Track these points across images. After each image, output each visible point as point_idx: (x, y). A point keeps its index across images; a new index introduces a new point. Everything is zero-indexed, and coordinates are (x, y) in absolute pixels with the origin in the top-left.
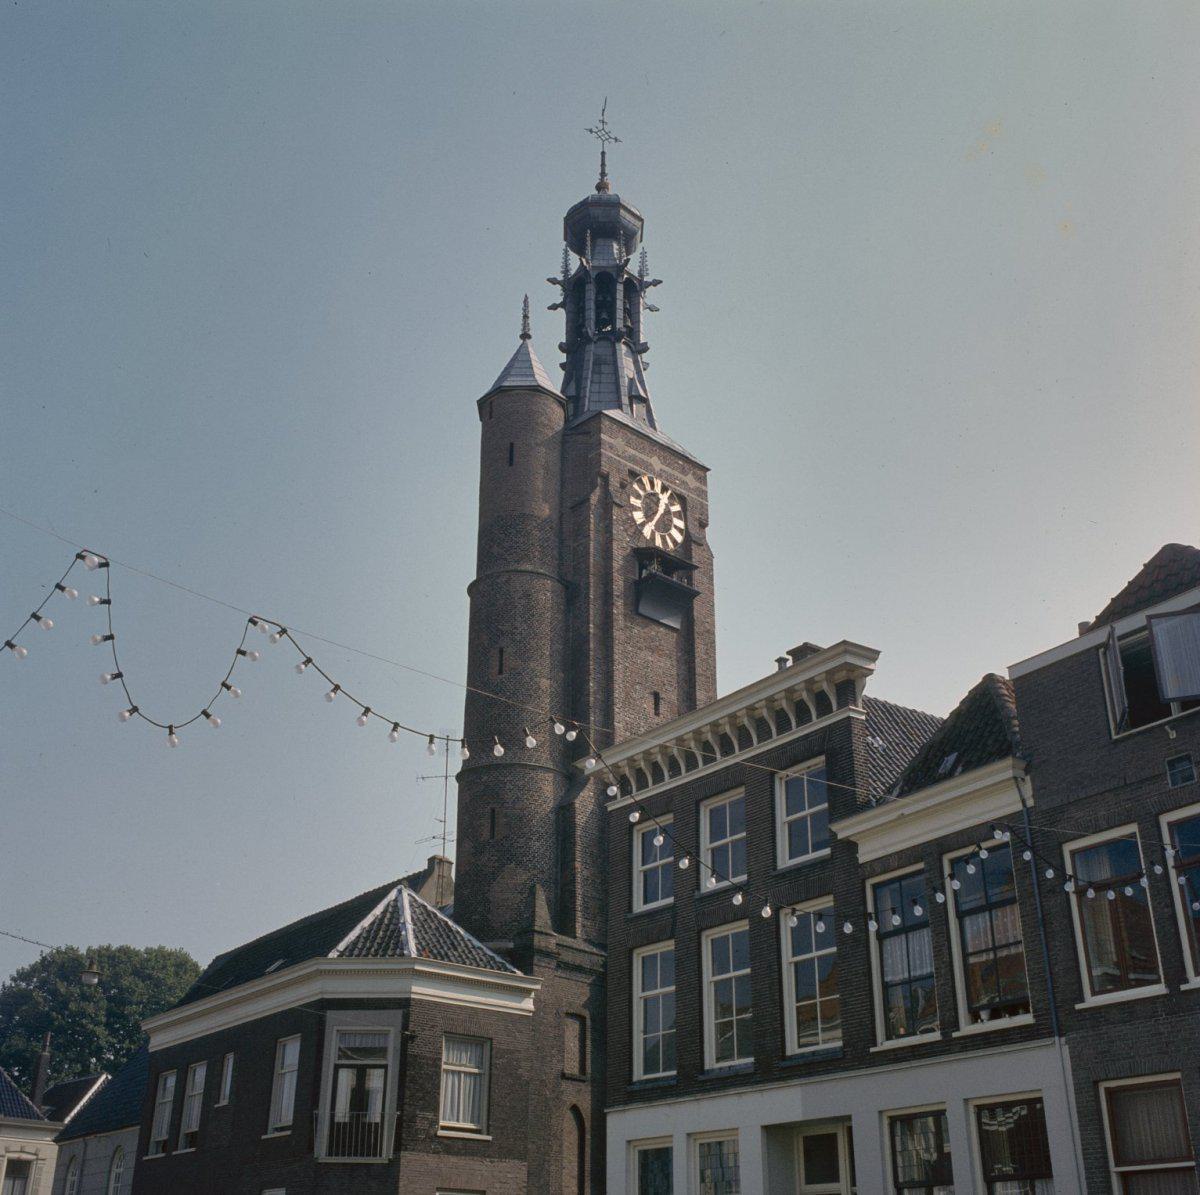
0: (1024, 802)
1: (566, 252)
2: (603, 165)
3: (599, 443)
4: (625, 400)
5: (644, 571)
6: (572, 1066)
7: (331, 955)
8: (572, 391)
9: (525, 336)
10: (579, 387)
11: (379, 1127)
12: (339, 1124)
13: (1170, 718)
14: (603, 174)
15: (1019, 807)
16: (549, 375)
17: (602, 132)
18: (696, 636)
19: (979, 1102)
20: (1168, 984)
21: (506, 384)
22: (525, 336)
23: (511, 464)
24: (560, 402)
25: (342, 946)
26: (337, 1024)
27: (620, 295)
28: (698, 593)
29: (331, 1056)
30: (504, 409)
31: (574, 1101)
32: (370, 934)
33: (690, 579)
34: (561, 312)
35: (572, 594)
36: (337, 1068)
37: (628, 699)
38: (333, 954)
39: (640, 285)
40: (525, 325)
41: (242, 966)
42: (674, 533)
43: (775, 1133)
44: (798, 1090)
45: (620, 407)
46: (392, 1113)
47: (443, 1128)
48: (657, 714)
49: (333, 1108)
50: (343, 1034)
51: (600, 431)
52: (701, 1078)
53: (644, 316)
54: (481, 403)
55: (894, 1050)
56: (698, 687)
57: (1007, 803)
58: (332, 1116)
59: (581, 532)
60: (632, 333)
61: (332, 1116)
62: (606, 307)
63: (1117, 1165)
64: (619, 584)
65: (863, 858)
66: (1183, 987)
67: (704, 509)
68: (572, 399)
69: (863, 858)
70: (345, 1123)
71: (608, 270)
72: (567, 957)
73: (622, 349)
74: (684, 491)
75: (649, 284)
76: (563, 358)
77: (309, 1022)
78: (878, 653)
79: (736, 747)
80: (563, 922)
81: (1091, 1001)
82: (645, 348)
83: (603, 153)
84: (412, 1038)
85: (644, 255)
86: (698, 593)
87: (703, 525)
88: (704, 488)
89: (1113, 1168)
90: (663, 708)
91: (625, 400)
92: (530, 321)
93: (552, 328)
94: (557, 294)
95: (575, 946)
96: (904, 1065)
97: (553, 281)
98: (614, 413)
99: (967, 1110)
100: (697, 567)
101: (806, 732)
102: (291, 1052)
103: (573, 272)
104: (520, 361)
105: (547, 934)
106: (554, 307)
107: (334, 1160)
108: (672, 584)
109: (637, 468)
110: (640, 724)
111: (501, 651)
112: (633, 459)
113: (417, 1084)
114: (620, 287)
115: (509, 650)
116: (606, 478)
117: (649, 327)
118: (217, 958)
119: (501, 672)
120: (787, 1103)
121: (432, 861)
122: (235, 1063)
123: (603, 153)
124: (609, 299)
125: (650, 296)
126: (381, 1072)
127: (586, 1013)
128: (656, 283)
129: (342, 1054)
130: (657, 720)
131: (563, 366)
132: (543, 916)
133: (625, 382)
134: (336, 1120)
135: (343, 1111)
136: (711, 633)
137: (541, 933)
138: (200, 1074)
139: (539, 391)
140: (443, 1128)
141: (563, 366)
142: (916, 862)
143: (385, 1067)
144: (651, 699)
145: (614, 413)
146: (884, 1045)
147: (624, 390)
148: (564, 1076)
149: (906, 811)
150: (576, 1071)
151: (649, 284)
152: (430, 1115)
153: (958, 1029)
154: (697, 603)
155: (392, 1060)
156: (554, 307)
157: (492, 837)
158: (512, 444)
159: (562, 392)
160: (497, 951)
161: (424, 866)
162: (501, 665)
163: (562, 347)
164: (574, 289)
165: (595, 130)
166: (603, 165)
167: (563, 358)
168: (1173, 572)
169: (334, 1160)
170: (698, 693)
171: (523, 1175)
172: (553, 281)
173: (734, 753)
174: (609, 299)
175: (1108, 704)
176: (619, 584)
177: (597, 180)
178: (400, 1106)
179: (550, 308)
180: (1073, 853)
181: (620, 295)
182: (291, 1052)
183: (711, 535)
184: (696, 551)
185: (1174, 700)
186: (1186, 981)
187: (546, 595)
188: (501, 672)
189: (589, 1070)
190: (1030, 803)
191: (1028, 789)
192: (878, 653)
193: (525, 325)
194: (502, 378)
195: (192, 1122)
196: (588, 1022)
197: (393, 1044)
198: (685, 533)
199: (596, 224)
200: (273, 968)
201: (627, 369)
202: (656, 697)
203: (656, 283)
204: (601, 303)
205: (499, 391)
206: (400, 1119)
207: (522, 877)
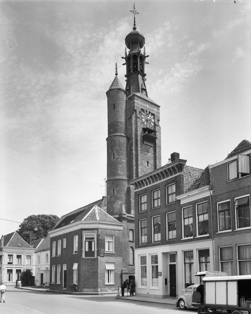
0: (211, 194)
1: (126, 49)
2: (135, 22)
3: (134, 102)
4: (140, 90)
5: (145, 133)
6: (131, 239)
7: (82, 220)
8: (128, 88)
9: (116, 74)
10: (130, 87)
11: (94, 252)
12: (86, 251)
13: (130, 275)
14: (135, 25)
15: (210, 195)
16: (123, 85)
17: (134, 12)
18: (157, 148)
19: (199, 249)
20: (232, 230)
21: (112, 88)
22: (116, 74)
23: (114, 109)
24: (125, 92)
25: (84, 218)
26: (85, 235)
27: (139, 61)
28: (157, 138)
29: (84, 240)
30: (112, 94)
31: (131, 246)
32: (90, 216)
33: (155, 134)
34: (125, 66)
35: (129, 139)
36: (85, 241)
37: (141, 163)
38: (83, 220)
39: (144, 57)
40: (116, 72)
41: (68, 219)
42: (152, 123)
43: (164, 254)
44: (169, 246)
45: (139, 92)
46: (96, 249)
47: (106, 252)
48: (148, 166)
49: (85, 249)
50: (86, 235)
51: (134, 99)
52: (151, 244)
53: (146, 66)
54: (107, 93)
55: (185, 240)
56: (157, 159)
57: (208, 194)
58: (85, 250)
59: (131, 124)
60: (142, 71)
61: (85, 250)
62: (135, 64)
63: (221, 261)
64: (139, 139)
65: (181, 203)
66: (235, 230)
67: (159, 117)
68: (128, 91)
69: (181, 203)
70: (87, 251)
71: (136, 54)
72: (129, 218)
73: (140, 77)
74: (154, 113)
75: (146, 57)
76: (126, 79)
77: (79, 232)
78: (186, 161)
79: (152, 183)
80: (128, 211)
81: (219, 232)
82: (145, 75)
83: (135, 18)
84: (99, 235)
85: (144, 48)
86: (157, 138)
87: (158, 121)
88: (159, 111)
89: (220, 261)
90: (149, 165)
91: (140, 90)
92: (117, 70)
93: (123, 70)
94: (124, 61)
95: (131, 216)
96: (187, 243)
97: (123, 58)
98: (138, 94)
99: (197, 251)
100: (157, 132)
101: (172, 177)
102: (76, 238)
103: (127, 55)
104: (116, 81)
105: (125, 214)
106: (124, 64)
107: (86, 258)
108: (150, 136)
109: (143, 108)
110: (144, 169)
111: (114, 154)
112: (142, 106)
113: (101, 244)
114: (139, 59)
115: (116, 154)
116: (136, 111)
117: (147, 69)
118: (125, 39)
119: (114, 159)
120: (167, 249)
121: (103, 197)
122: (67, 241)
123: (135, 18)
124: (136, 62)
125: (147, 60)
126: (94, 242)
127: (134, 229)
128: (148, 56)
129: (86, 239)
130: (148, 167)
131: (126, 80)
132: (124, 211)
133: (140, 85)
134: (86, 251)
135: (87, 250)
136: (160, 147)
137: (124, 214)
138: (60, 241)
139: (120, 90)
140: (106, 252)
141: (126, 80)
142: (191, 205)
143: (94, 241)
144: (147, 163)
145: (138, 94)
146: (183, 239)
147: (140, 87)
148: (130, 241)
149: (189, 195)
150: (132, 240)
151: (146, 57)
152: (103, 249)
153: (196, 236)
154: (157, 140)
155: (95, 240)
156: (124, 64)
157: (114, 194)
158: (114, 104)
159: (125, 89)
160: (115, 218)
161: (102, 198)
162: (114, 157)
163: (126, 76)
164: (128, 59)
165: (132, 11)
166: (135, 22)
167: (126, 79)
168: (243, 146)
169: (86, 258)
170: (157, 161)
171: (122, 260)
172: (123, 58)
173: (148, 185)
174: (136, 62)
175: (228, 173)
176: (139, 139)
177: (133, 27)
178: (98, 248)
179: (123, 65)
180: (219, 204)
181: (139, 61)
182: (76, 238)
183: (161, 123)
184: (157, 128)
185: (240, 173)
186: (235, 229)
187: (123, 141)
188: (114, 159)
189: (134, 240)
190: (212, 194)
191: (212, 191)
192: (186, 161)
193: (116, 72)
194: (111, 86)
195: (59, 253)
196: (134, 231)
197: (95, 237)
198: (154, 123)
199: (134, 40)
200: (71, 222)
201: (141, 82)
202: (148, 162)
203: (148, 56)
204: (135, 64)
205: (111, 90)
206: (98, 250)
207: (120, 202)
